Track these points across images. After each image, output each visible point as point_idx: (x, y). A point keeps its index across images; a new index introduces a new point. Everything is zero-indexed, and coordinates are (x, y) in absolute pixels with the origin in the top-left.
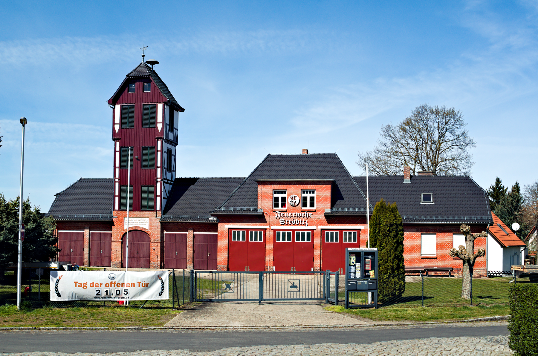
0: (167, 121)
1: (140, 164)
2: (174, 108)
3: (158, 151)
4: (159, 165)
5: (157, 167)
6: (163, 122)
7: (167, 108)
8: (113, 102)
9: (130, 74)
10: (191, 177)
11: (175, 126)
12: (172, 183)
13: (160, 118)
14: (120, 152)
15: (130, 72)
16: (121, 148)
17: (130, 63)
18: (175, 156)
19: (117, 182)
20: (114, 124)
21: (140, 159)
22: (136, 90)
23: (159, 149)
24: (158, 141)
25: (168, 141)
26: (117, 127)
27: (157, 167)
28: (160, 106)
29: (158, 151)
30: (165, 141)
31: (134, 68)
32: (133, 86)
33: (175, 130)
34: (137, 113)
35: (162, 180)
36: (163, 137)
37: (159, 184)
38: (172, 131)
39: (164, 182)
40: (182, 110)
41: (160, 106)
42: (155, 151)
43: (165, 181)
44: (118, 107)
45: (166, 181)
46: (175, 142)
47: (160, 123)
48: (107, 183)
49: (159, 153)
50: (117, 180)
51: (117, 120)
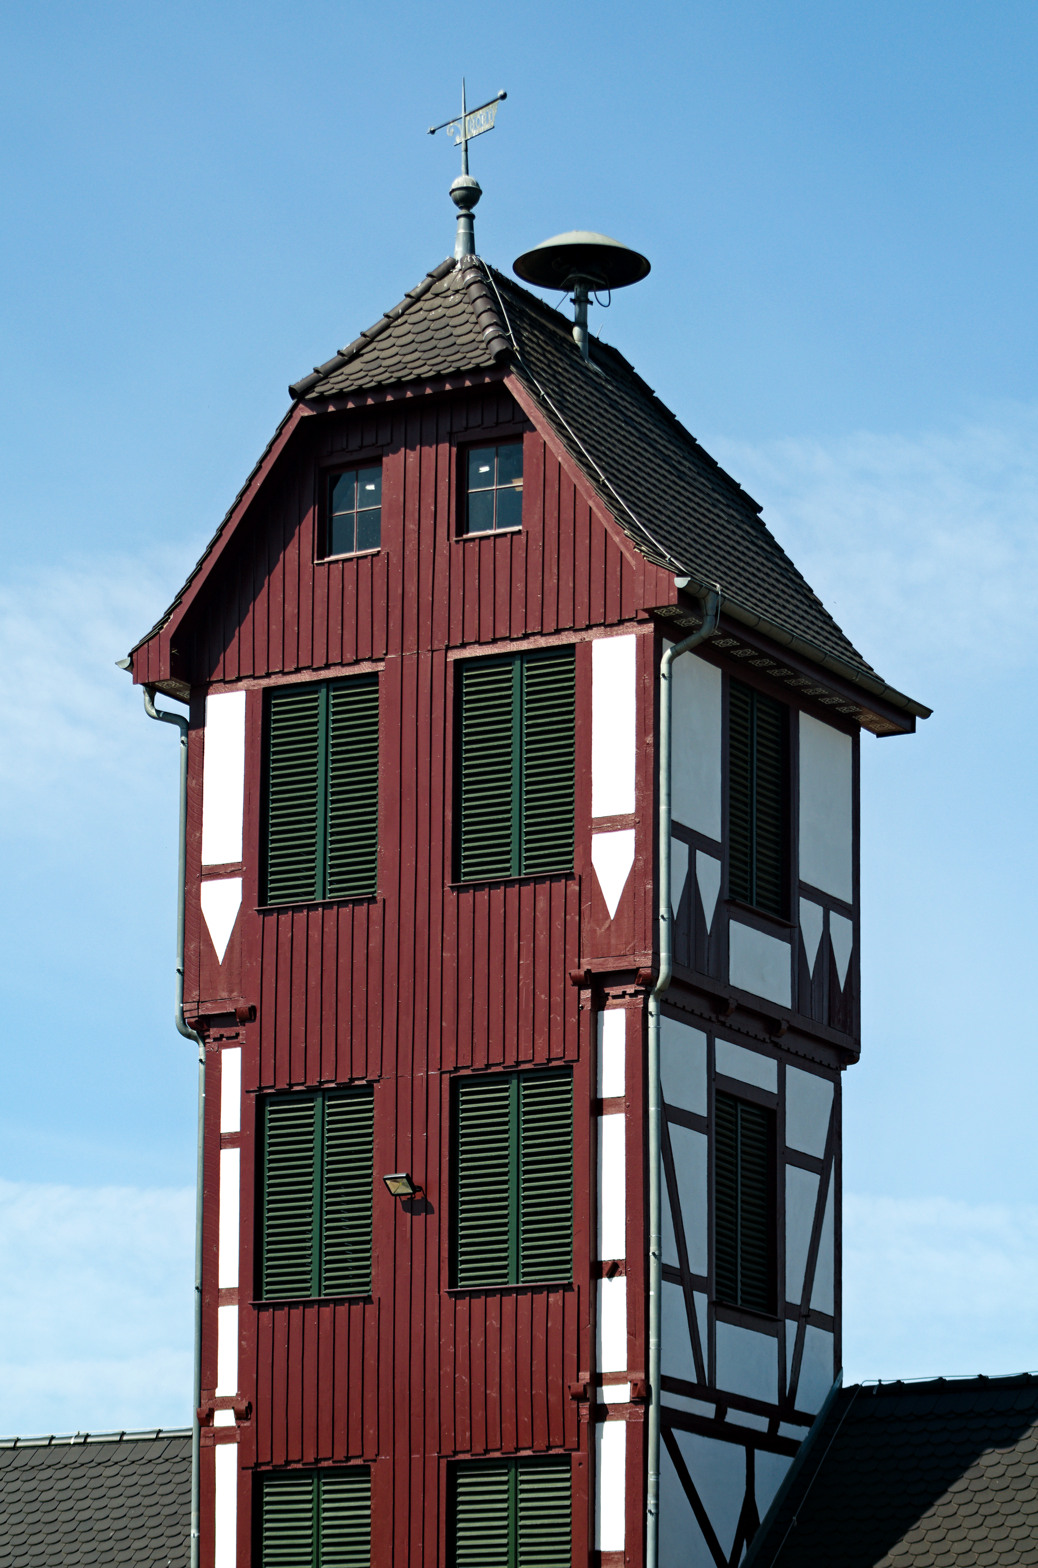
0: (701, 801)
1: (438, 1246)
2: (787, 683)
3: (598, 1107)
4: (613, 1245)
5: (599, 1270)
6: (645, 821)
7: (699, 690)
8: (185, 657)
9: (323, 375)
10: (995, 1370)
11: (816, 863)
12: (797, 1433)
13: (612, 782)
14: (256, 1141)
15: (326, 357)
16: (259, 1101)
17: (340, 283)
18: (828, 1165)
19: (225, 1436)
20: (195, 872)
21: (439, 1198)
22: (389, 525)
23: (613, 1083)
24: (600, 1004)
25: (702, 997)
26: (223, 905)
27: (599, 1270)
28: (614, 662)
29: (598, 1107)
30: (667, 1009)
31: (373, 320)
32: (365, 495)
33: (809, 913)
34: (409, 752)
35: (641, 1397)
36: (644, 962)
37: (613, 1438)
38: (781, 921)
39: (669, 1419)
40: (901, 715)
41: (614, 662)
42: (580, 1108)
43: (682, 1412)
44: (227, 712)
45: (706, 1410)
46: (824, 1026)
47: (613, 824)
48: (152, 1471)
49: (613, 1128)
50: (224, 1418)
51: (224, 838)
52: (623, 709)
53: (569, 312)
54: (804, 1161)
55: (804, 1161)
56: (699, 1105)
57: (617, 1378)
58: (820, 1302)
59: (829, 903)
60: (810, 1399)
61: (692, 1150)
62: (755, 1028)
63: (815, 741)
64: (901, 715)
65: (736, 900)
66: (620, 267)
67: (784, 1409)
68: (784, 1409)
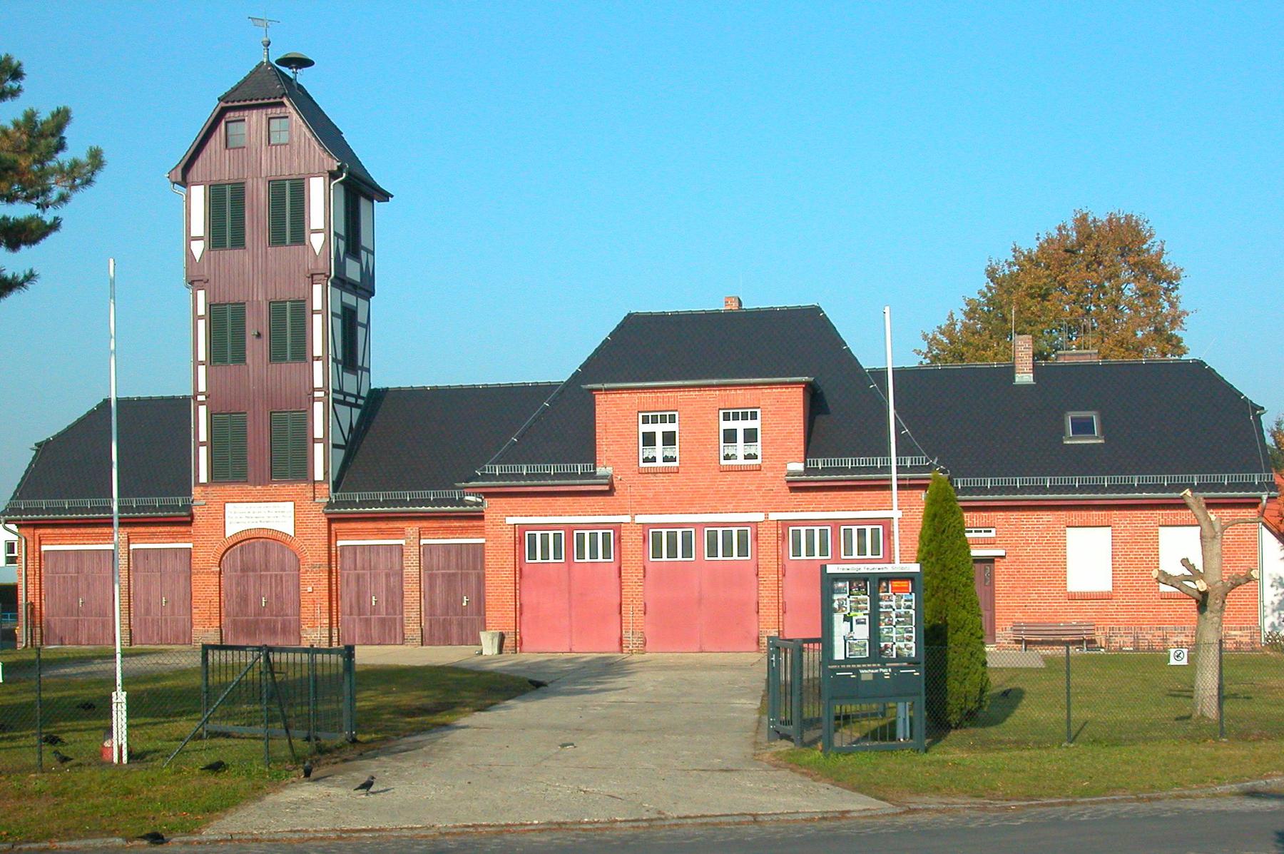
2: (358, 190)
5: (314, 441)
11: (365, 241)
16: (210, 306)
18: (367, 326)
26: (198, 248)
27: (314, 441)
33: (363, 254)
40: (385, 196)
52: (320, 201)
53: (292, 76)
54: (362, 325)
55: (362, 325)
56: (339, 312)
57: (319, 390)
58: (366, 365)
59: (368, 251)
60: (364, 393)
61: (338, 322)
62: (350, 287)
63: (364, 203)
64: (385, 196)
65: (347, 252)
66: (304, 63)
67: (358, 396)
68: (358, 396)
